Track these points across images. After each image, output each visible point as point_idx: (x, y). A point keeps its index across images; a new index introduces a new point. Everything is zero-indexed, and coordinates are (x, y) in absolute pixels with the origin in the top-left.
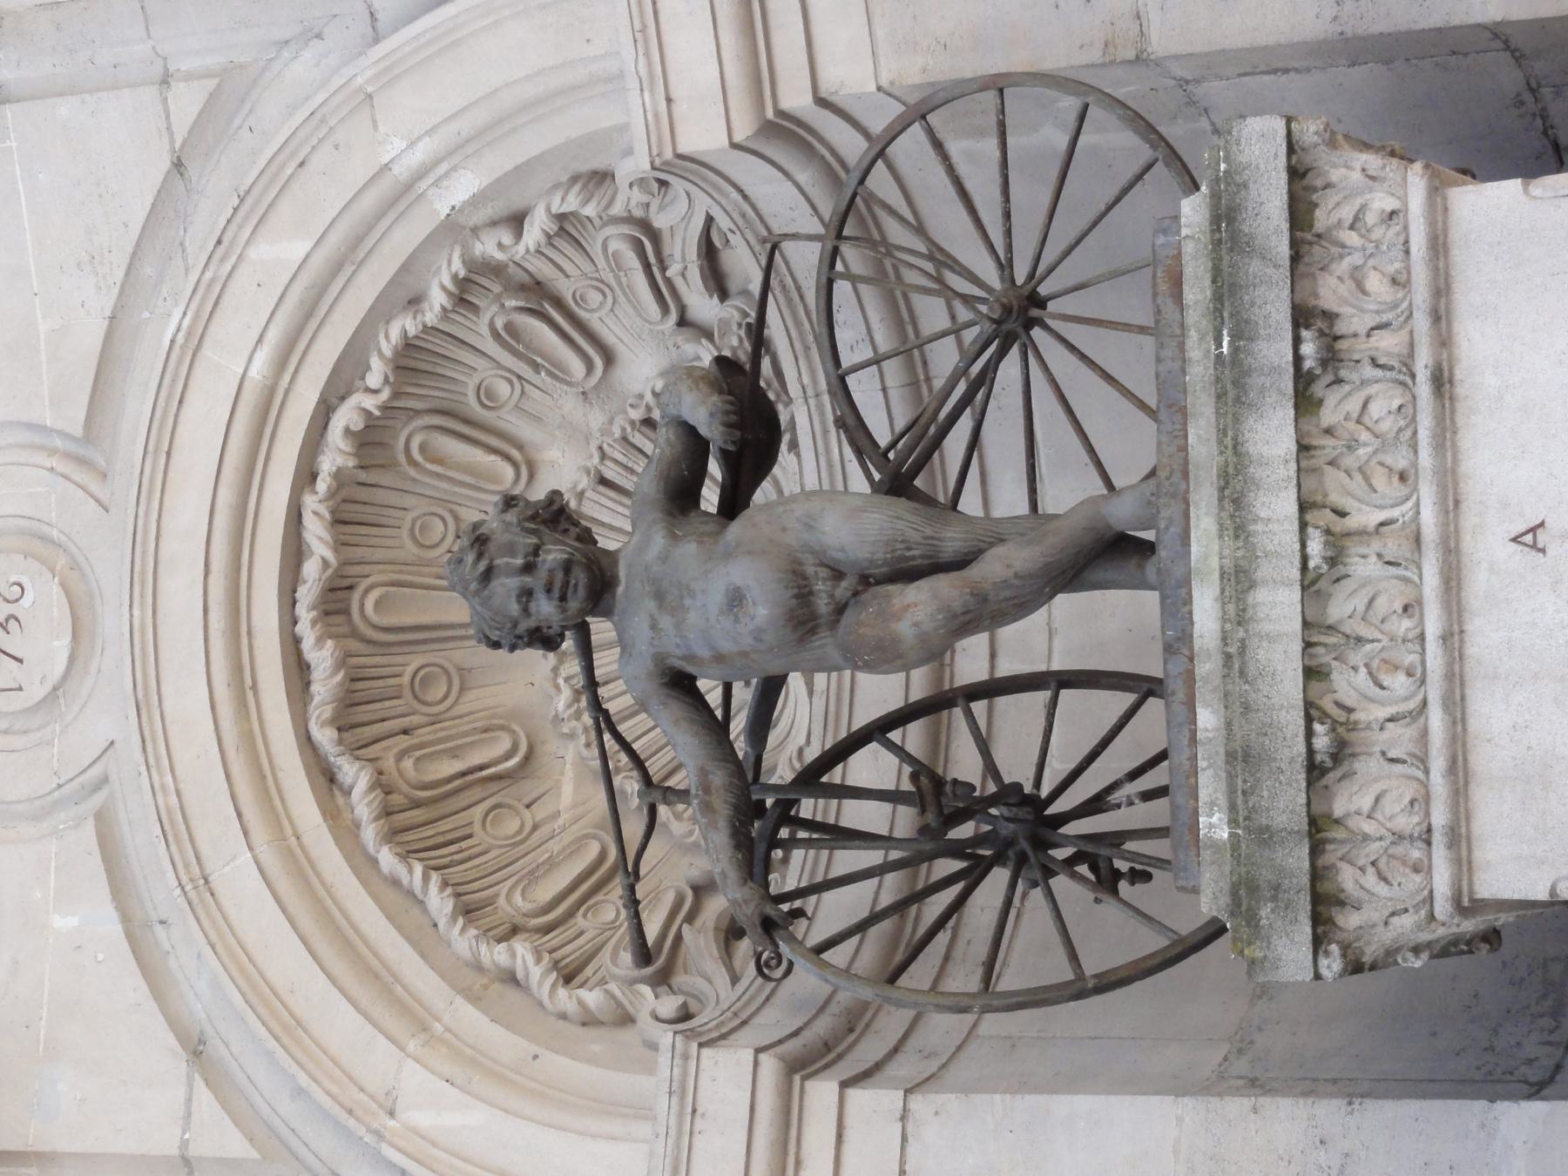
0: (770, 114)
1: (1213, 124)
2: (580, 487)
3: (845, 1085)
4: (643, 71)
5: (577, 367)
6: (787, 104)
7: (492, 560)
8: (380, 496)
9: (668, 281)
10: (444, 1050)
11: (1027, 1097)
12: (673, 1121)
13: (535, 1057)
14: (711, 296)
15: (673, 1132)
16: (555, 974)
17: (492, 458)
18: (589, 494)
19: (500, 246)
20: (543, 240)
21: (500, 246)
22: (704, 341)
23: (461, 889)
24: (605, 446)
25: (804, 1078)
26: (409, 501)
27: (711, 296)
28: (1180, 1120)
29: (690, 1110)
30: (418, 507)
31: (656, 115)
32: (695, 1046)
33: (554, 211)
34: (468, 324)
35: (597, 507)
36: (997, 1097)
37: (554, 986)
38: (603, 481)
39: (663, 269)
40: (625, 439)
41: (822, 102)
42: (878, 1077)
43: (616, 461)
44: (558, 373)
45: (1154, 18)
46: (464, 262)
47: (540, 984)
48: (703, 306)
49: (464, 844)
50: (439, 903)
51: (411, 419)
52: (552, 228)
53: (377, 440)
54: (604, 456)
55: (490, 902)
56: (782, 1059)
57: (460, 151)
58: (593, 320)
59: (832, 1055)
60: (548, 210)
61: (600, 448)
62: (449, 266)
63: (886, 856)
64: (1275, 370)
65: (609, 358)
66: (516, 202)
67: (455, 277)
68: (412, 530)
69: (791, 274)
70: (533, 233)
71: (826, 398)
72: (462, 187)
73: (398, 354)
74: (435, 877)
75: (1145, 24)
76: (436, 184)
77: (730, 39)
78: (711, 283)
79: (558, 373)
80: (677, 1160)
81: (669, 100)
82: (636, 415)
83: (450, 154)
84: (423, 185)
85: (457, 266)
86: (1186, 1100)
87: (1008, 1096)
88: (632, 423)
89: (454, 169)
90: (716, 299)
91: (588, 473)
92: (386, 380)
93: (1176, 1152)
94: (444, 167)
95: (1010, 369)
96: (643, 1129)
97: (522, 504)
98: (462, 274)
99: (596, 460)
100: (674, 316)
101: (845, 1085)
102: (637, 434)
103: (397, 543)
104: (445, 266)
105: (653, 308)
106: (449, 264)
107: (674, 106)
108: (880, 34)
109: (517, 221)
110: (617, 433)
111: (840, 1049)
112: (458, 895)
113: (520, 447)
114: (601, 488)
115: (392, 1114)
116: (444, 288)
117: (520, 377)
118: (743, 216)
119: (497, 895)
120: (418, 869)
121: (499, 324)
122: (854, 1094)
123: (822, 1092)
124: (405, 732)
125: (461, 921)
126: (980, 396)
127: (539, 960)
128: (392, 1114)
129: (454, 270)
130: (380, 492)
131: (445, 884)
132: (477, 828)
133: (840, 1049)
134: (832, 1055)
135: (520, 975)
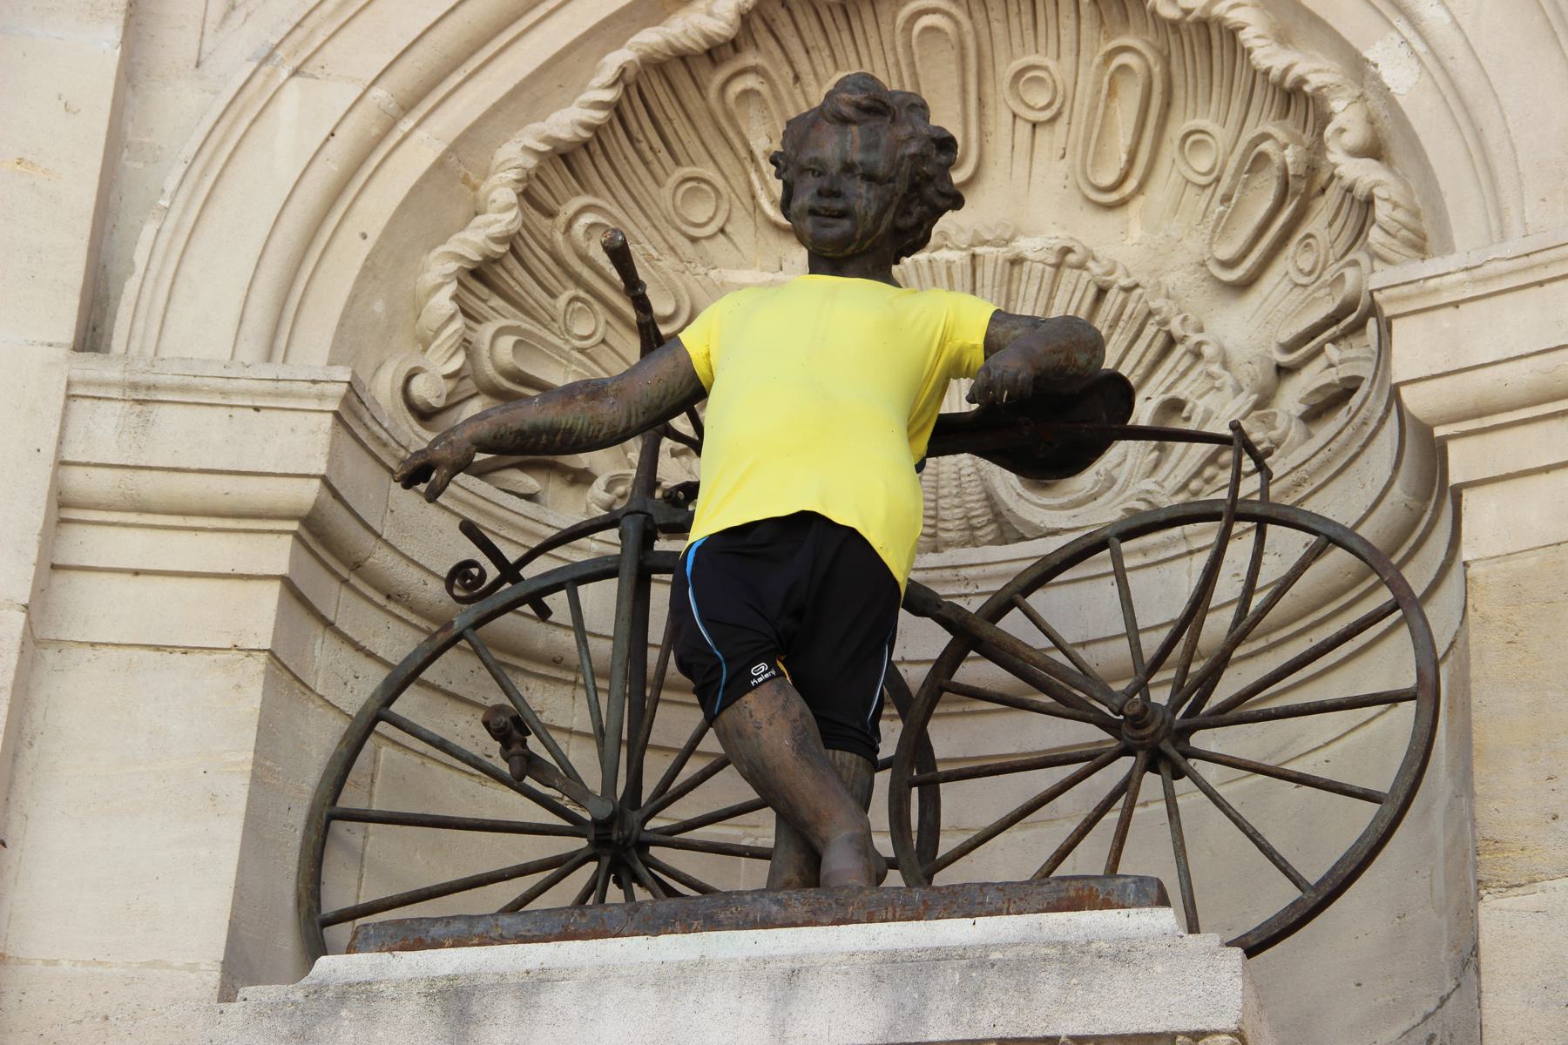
0: (1439, 432)
1: (1449, 996)
2: (1091, 264)
3: (286, 581)
4: (1488, 269)
5: (1226, 251)
6: (1454, 449)
7: (854, 122)
8: (1068, 23)
9: (1319, 351)
10: (375, 131)
11: (245, 791)
12: (243, 384)
13: (364, 236)
14: (1301, 401)
15: (234, 384)
16: (479, 259)
17: (1124, 157)
18: (1085, 274)
19: (1342, 131)
20: (1346, 182)
21: (1342, 131)
22: (1255, 397)
23: (595, 147)
24: (1138, 291)
25: (296, 535)
26: (1068, 59)
27: (1301, 401)
28: (193, 968)
29: (257, 404)
30: (1060, 70)
31: (1436, 290)
32: (336, 408)
33: (1376, 191)
34: (1266, 108)
35: (1071, 288)
36: (251, 755)
37: (462, 257)
38: (1102, 292)
39: (1334, 341)
40: (1150, 314)
41: (1457, 493)
42: (298, 611)
43: (1123, 306)
44: (1222, 228)
45: (1511, 901)
46: (1319, 89)
47: (465, 241)
48: (1292, 397)
49: (664, 154)
50: (567, 120)
51: (1159, 52)
52: (1360, 191)
53: (1130, 13)
54: (1128, 290)
55: (585, 186)
56: (316, 508)
57: (1435, 60)
58: (1284, 263)
59: (345, 573)
60: (1377, 184)
61: (1137, 286)
62: (1314, 68)
63: (655, 646)
64: (917, 1016)
65: (1244, 286)
66: (1396, 147)
67: (1301, 81)
68: (1045, 68)
69: (1315, 492)
70: (1361, 173)
71: (140, 257)
72: (1397, 70)
73: (1220, 21)
74: (599, 116)
75: (1520, 890)
76: (1405, 41)
77: (1521, 376)
78: (1319, 399)
79: (1222, 228)
80: (197, 390)
81: (1456, 304)
82: (1175, 327)
83: (1432, 51)
84: (1402, 25)
85: (1314, 81)
86: (217, 975)
87: (250, 767)
88: (1165, 322)
89: (1420, 61)
90: (1303, 408)
91: (1110, 273)
92: (1187, 12)
93: (152, 964)
94: (1420, 47)
95: (1086, 734)
96: (250, 351)
97: (943, 158)
98: (1307, 88)
99: (1125, 282)
100: (1285, 359)
101: (286, 581)
102: (1155, 329)
103: (1017, 50)
104: (1315, 66)
105: (1286, 336)
106: (1317, 71)
107: (1451, 310)
108: (1532, 560)
109: (1374, 150)
110: (1153, 305)
111: (354, 580)
112: (585, 145)
113: (1140, 189)
114: (1092, 291)
115: (296, 72)
116: (1286, 71)
117: (1218, 180)
118: (1364, 423)
119: (596, 195)
120: (609, 96)
121: (1266, 146)
122: (276, 586)
123: (276, 553)
124: (797, 78)
125: (543, 148)
126: (1045, 699)
127: (498, 240)
128: (296, 72)
129: (1310, 77)
130: (1072, 23)
131: (596, 129)
132: (687, 171)
133: (354, 580)
134: (345, 573)
135: (479, 220)
